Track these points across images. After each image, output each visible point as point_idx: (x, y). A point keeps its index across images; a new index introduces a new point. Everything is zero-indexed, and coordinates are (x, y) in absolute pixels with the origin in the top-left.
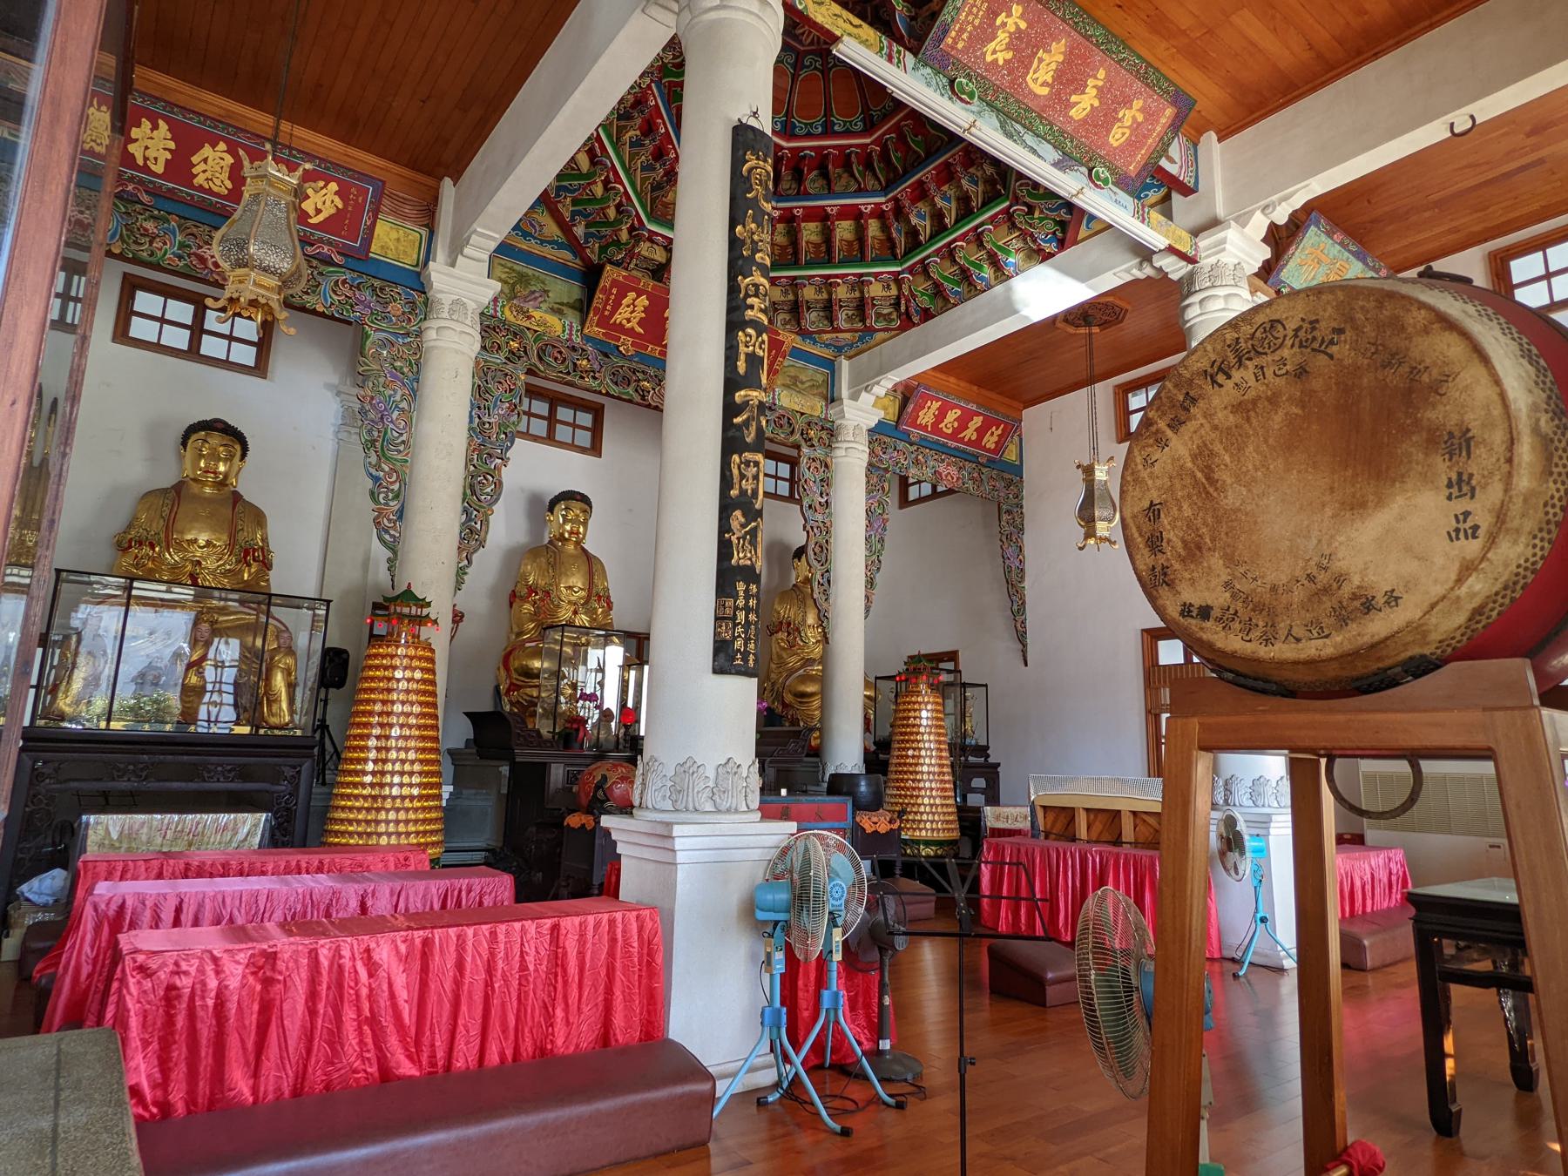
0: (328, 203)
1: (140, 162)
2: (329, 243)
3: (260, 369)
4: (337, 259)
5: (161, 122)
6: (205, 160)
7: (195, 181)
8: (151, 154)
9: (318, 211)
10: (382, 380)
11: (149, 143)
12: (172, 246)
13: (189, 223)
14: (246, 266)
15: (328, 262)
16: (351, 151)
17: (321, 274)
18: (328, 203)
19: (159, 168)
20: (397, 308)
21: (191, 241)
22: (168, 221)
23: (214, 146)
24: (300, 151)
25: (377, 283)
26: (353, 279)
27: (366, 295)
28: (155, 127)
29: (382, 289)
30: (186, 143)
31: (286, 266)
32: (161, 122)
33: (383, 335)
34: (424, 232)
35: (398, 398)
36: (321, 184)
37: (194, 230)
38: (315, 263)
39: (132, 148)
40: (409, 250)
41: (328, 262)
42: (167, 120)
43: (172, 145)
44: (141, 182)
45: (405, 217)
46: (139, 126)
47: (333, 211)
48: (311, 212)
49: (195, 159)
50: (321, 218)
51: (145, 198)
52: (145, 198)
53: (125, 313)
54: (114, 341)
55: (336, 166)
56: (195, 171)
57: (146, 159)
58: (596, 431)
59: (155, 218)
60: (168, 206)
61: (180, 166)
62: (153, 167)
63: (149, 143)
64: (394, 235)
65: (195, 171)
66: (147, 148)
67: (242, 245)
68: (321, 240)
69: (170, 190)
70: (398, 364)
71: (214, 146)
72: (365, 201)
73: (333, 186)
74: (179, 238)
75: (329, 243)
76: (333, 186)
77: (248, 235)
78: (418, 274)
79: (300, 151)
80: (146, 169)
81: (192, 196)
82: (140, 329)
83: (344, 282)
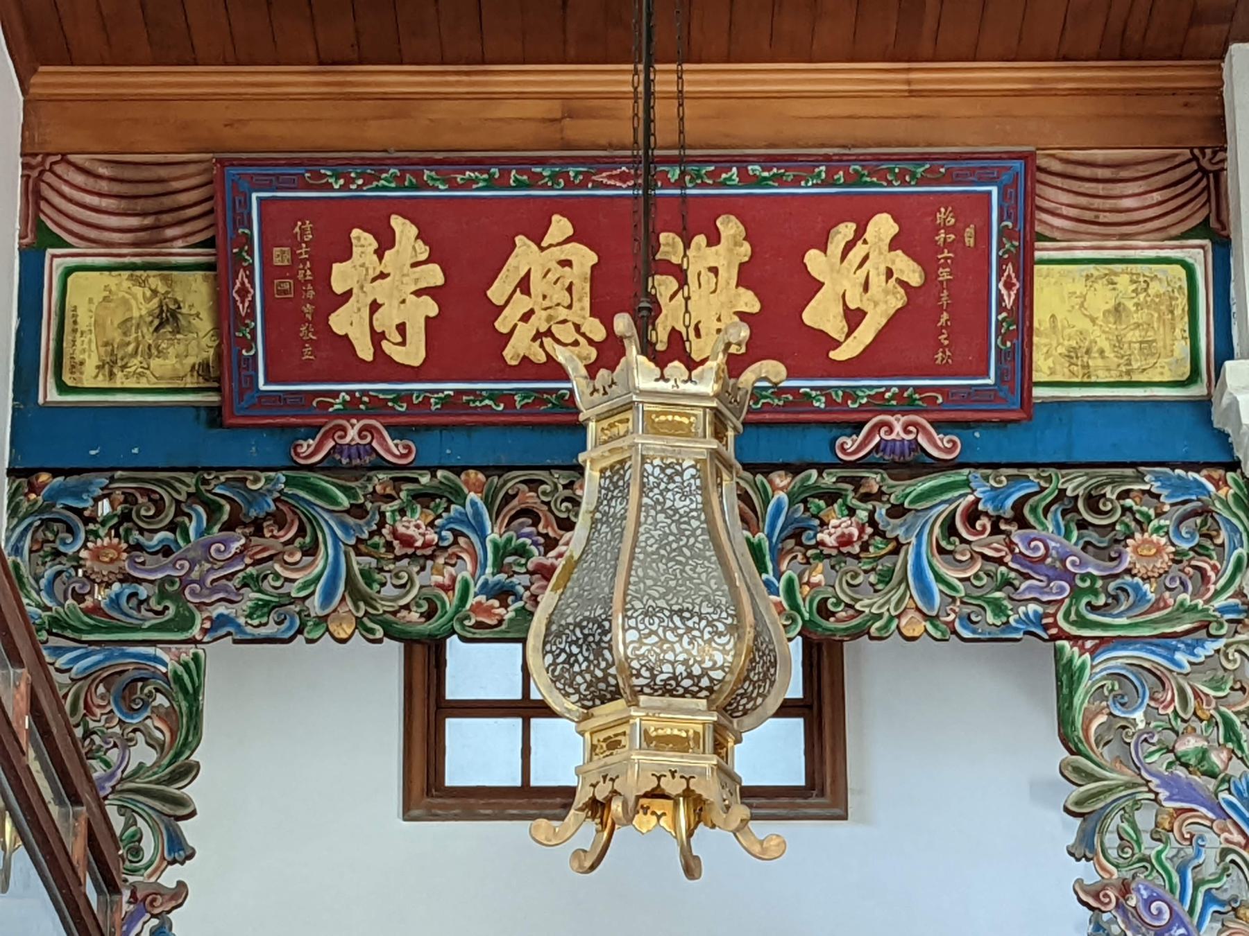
0: (877, 281)
1: (365, 352)
2: (905, 404)
3: (822, 789)
4: (938, 445)
5: (397, 222)
6: (524, 285)
7: (511, 354)
8: (387, 320)
9: (854, 318)
10: (1146, 819)
11: (379, 291)
12: (479, 565)
13: (513, 481)
14: (616, 694)
15: (913, 463)
16: (928, 75)
17: (897, 511)
18: (877, 281)
19: (413, 353)
20: (1146, 552)
21: (525, 534)
22: (457, 495)
23: (537, 237)
24: (767, 161)
25: (1075, 484)
26: (997, 496)
27: (1049, 536)
28: (386, 241)
29: (1093, 502)
30: (468, 260)
31: (718, 655)
32: (397, 222)
33: (1119, 658)
34: (1198, 254)
35: (1209, 860)
36: (846, 231)
37: (530, 499)
38: (874, 480)
39: (339, 322)
40: (1159, 335)
41: (913, 463)
42: (409, 210)
43: (434, 275)
44: (377, 406)
45: (1125, 228)
46: (346, 255)
47: (897, 301)
48: (834, 325)
49: (497, 293)
50: (866, 334)
51: (393, 448)
52: (393, 448)
53: (428, 709)
54: (407, 815)
55: (877, 164)
56: (502, 326)
57: (377, 338)
58: (820, 711)
59: (423, 498)
60: (453, 450)
61: (464, 329)
62: (399, 355)
63: (379, 291)
64: (1101, 299)
65: (502, 326)
66: (375, 307)
67: (595, 637)
68: (878, 404)
69: (452, 402)
70: (1189, 745)
71: (537, 237)
72: (983, 234)
73: (883, 226)
74: (494, 535)
75: (905, 404)
76: (883, 226)
77: (607, 603)
78: (1204, 406)
79: (767, 161)
80: (384, 367)
81: (506, 397)
82: (478, 753)
83: (972, 515)
